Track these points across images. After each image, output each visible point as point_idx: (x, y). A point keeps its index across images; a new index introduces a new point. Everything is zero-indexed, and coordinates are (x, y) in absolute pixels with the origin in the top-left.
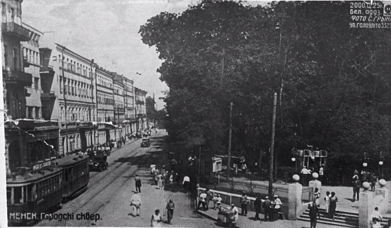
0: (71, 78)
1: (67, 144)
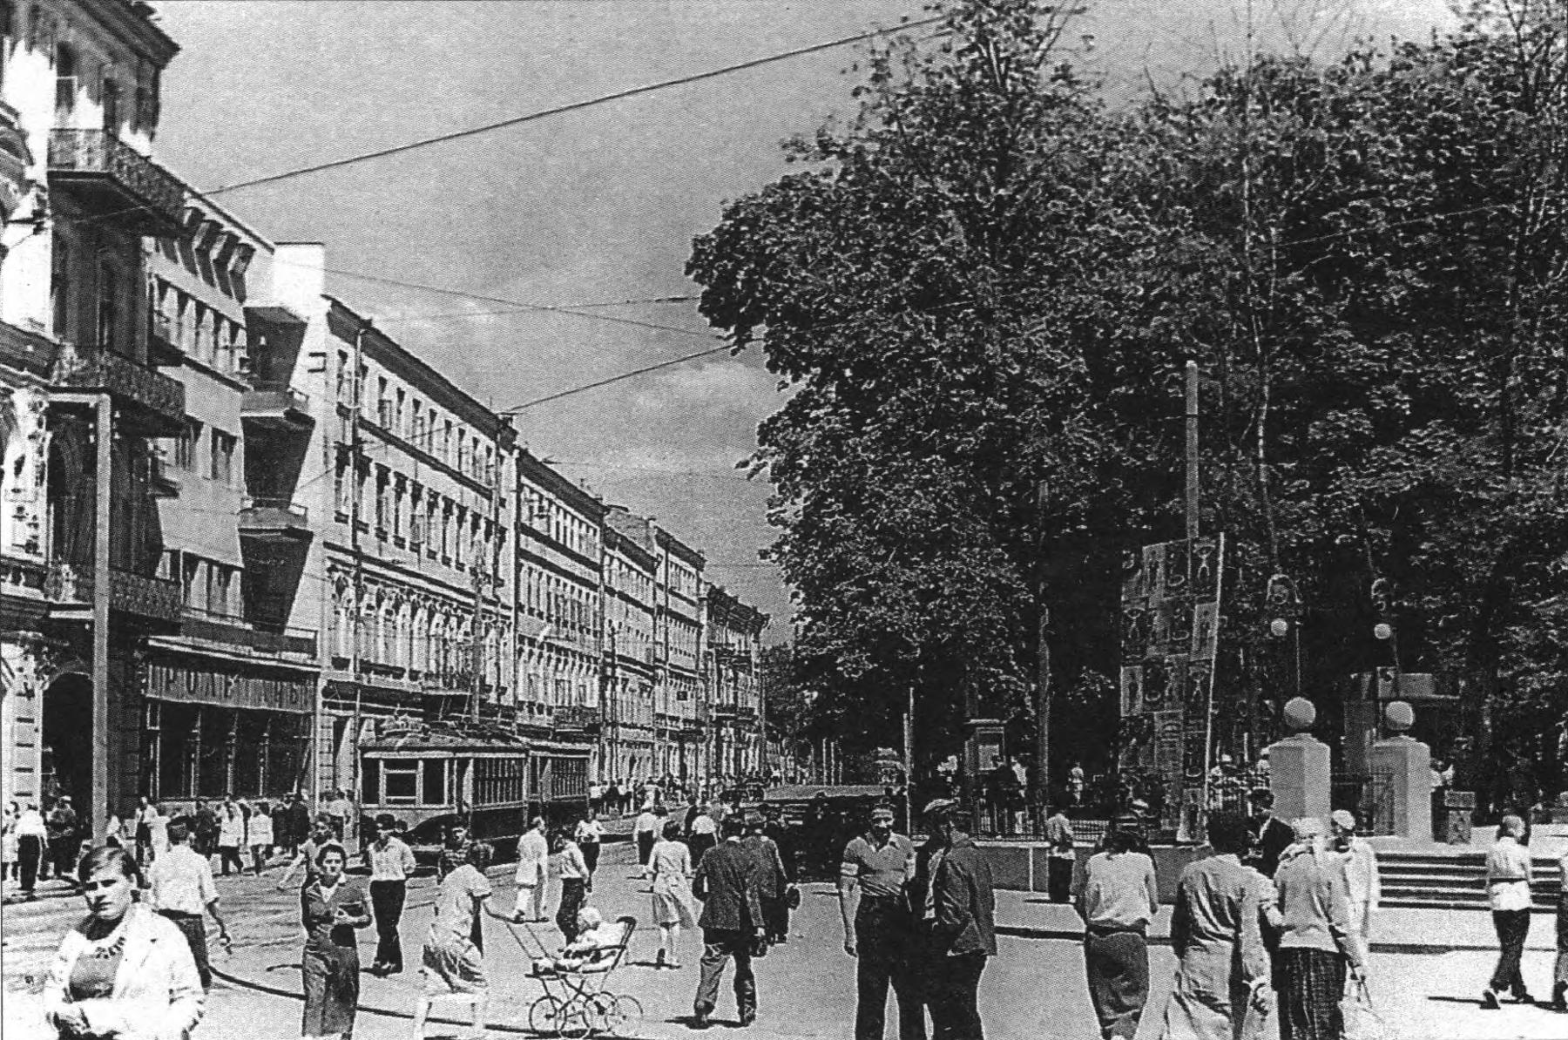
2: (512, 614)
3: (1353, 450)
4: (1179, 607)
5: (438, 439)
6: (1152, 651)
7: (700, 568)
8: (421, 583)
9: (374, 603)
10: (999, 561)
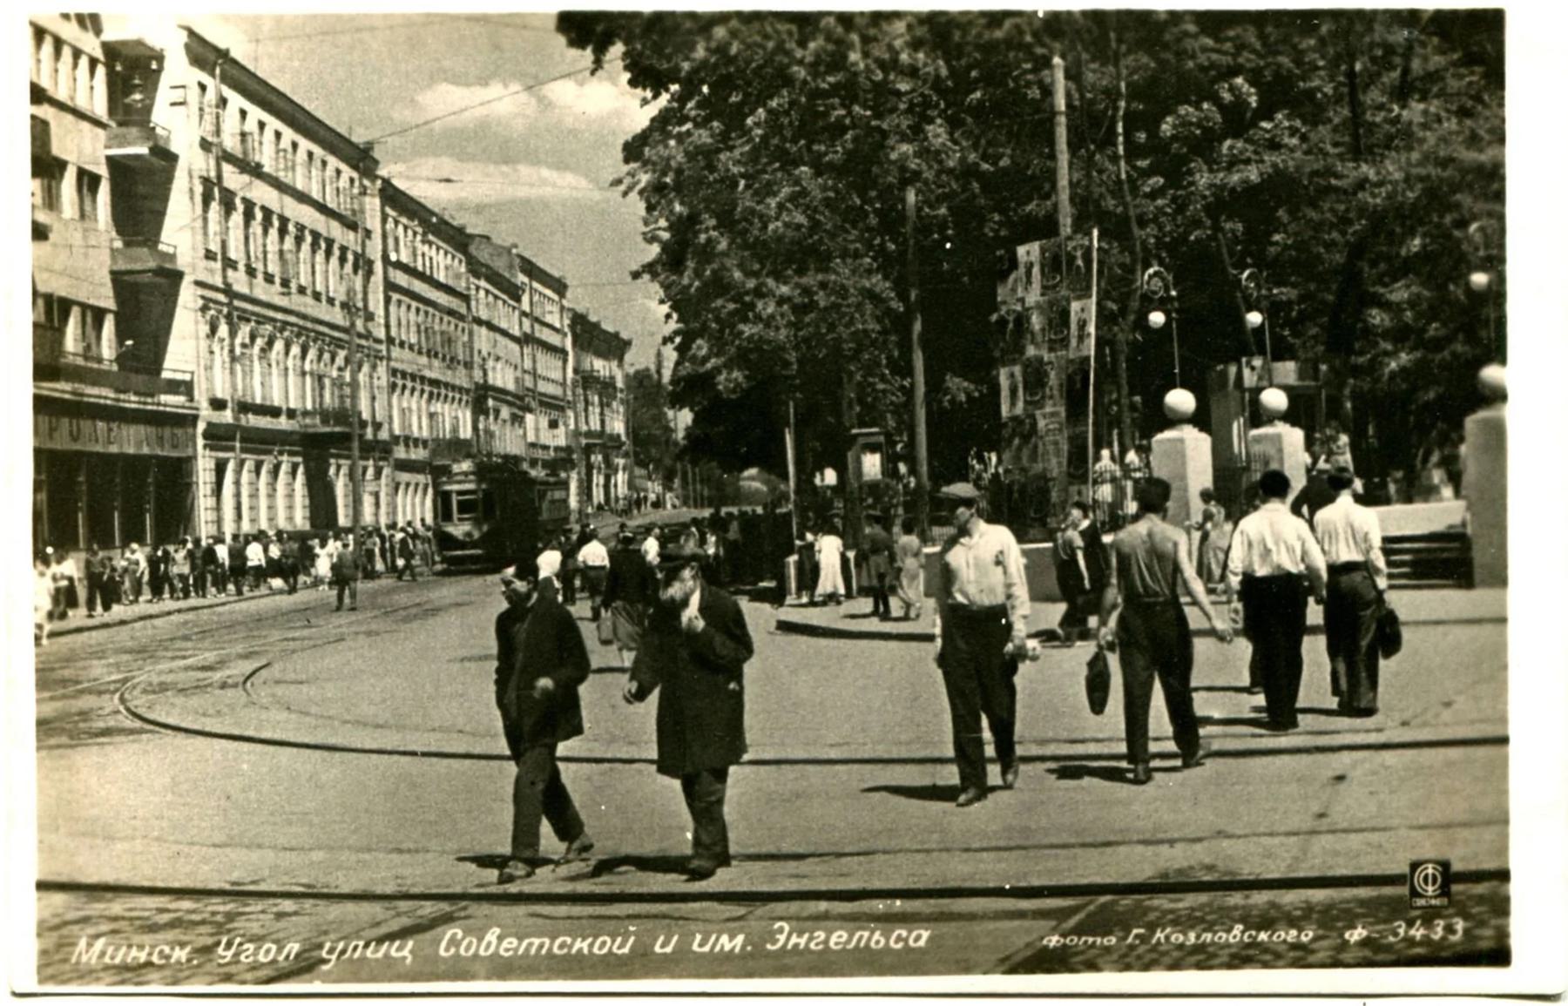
0: (275, 207)
1: (238, 495)
2: (383, 347)
3: (1203, 145)
4: (1053, 304)
5: (300, 170)
6: (1031, 351)
7: (562, 294)
8: (292, 319)
9: (247, 341)
10: (869, 272)
